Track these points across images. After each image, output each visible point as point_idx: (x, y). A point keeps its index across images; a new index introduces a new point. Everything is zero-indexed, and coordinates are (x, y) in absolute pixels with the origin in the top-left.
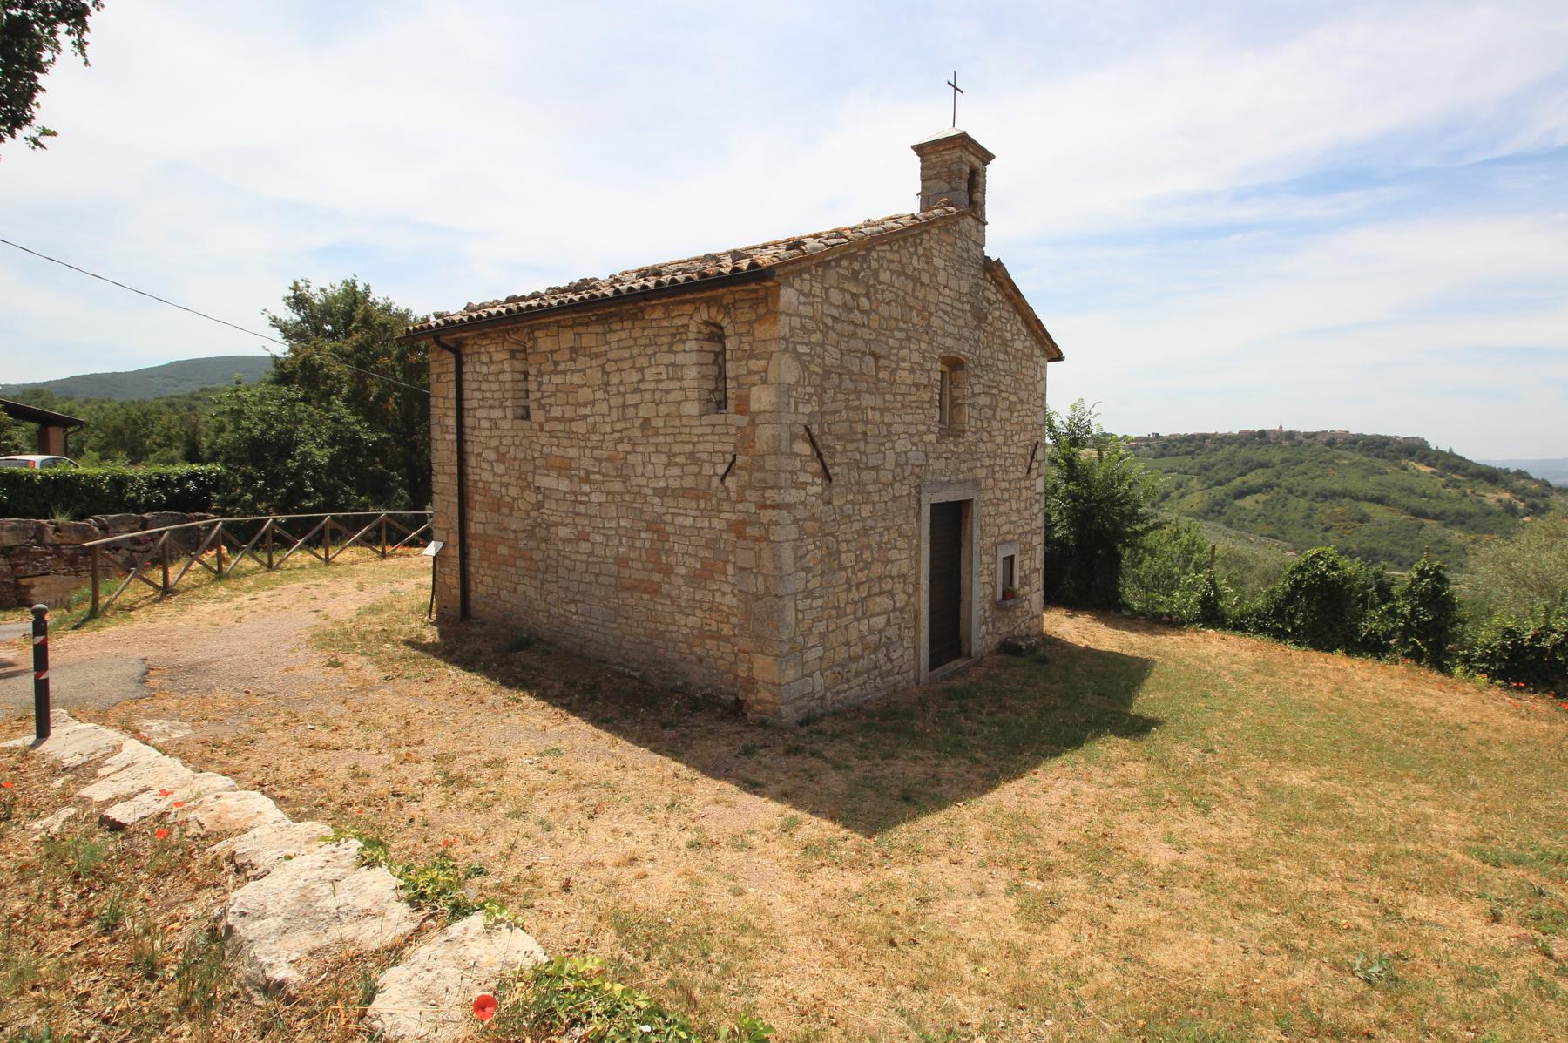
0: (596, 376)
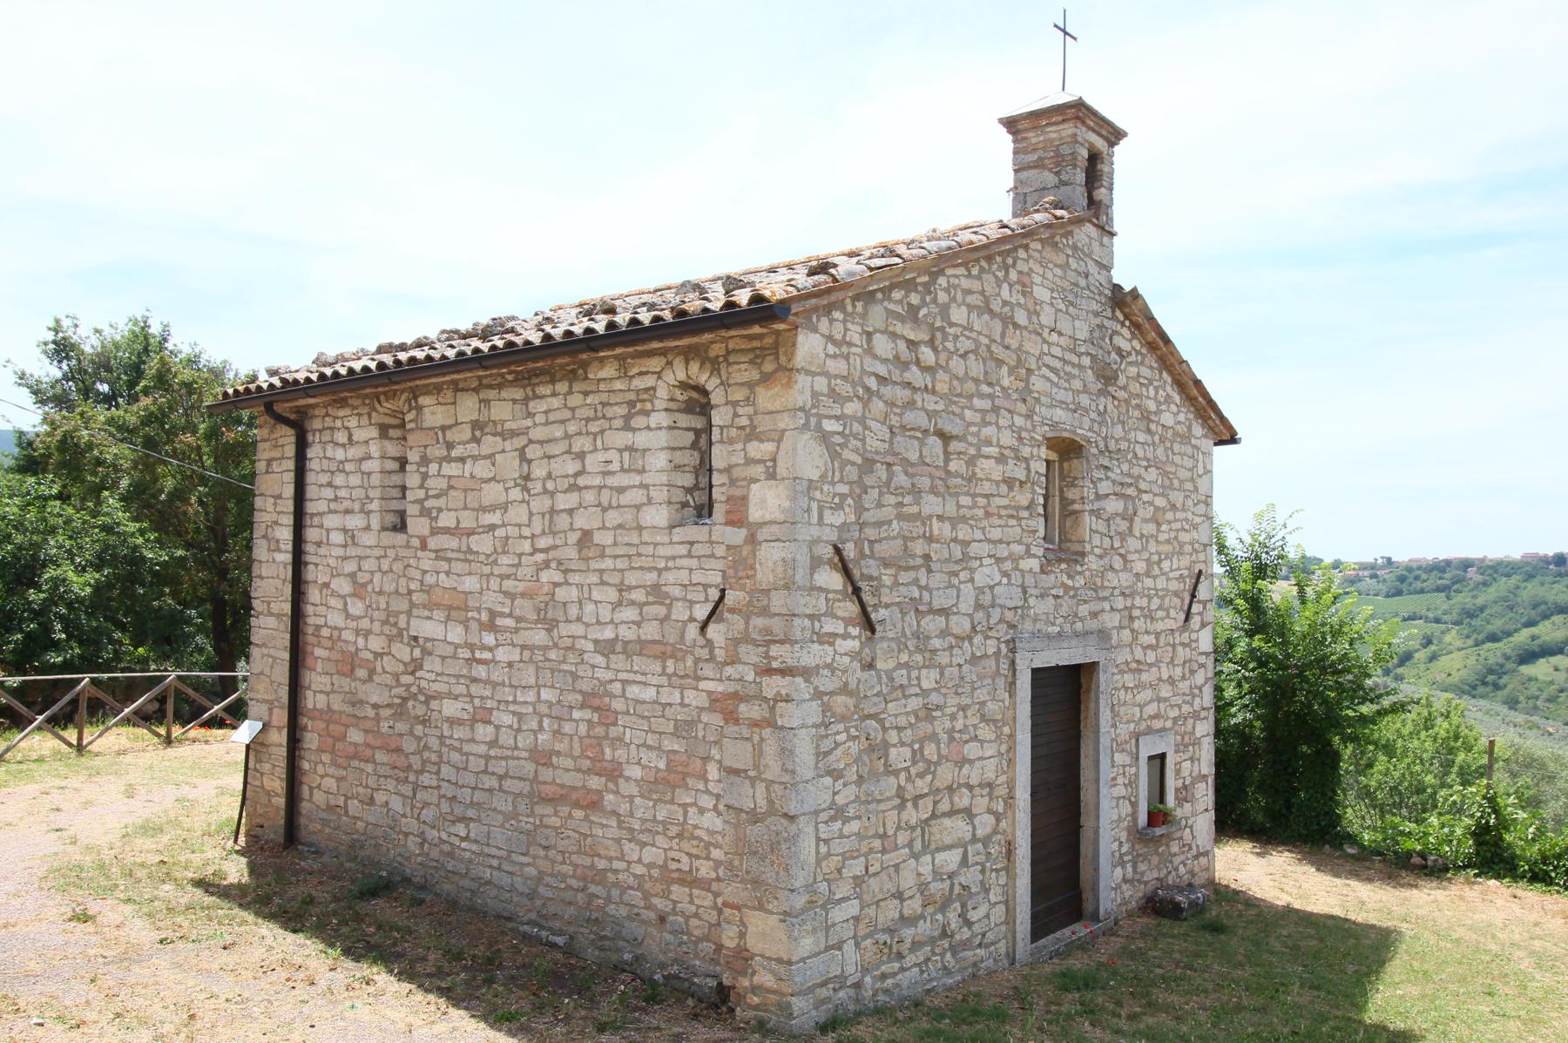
0: (510, 465)
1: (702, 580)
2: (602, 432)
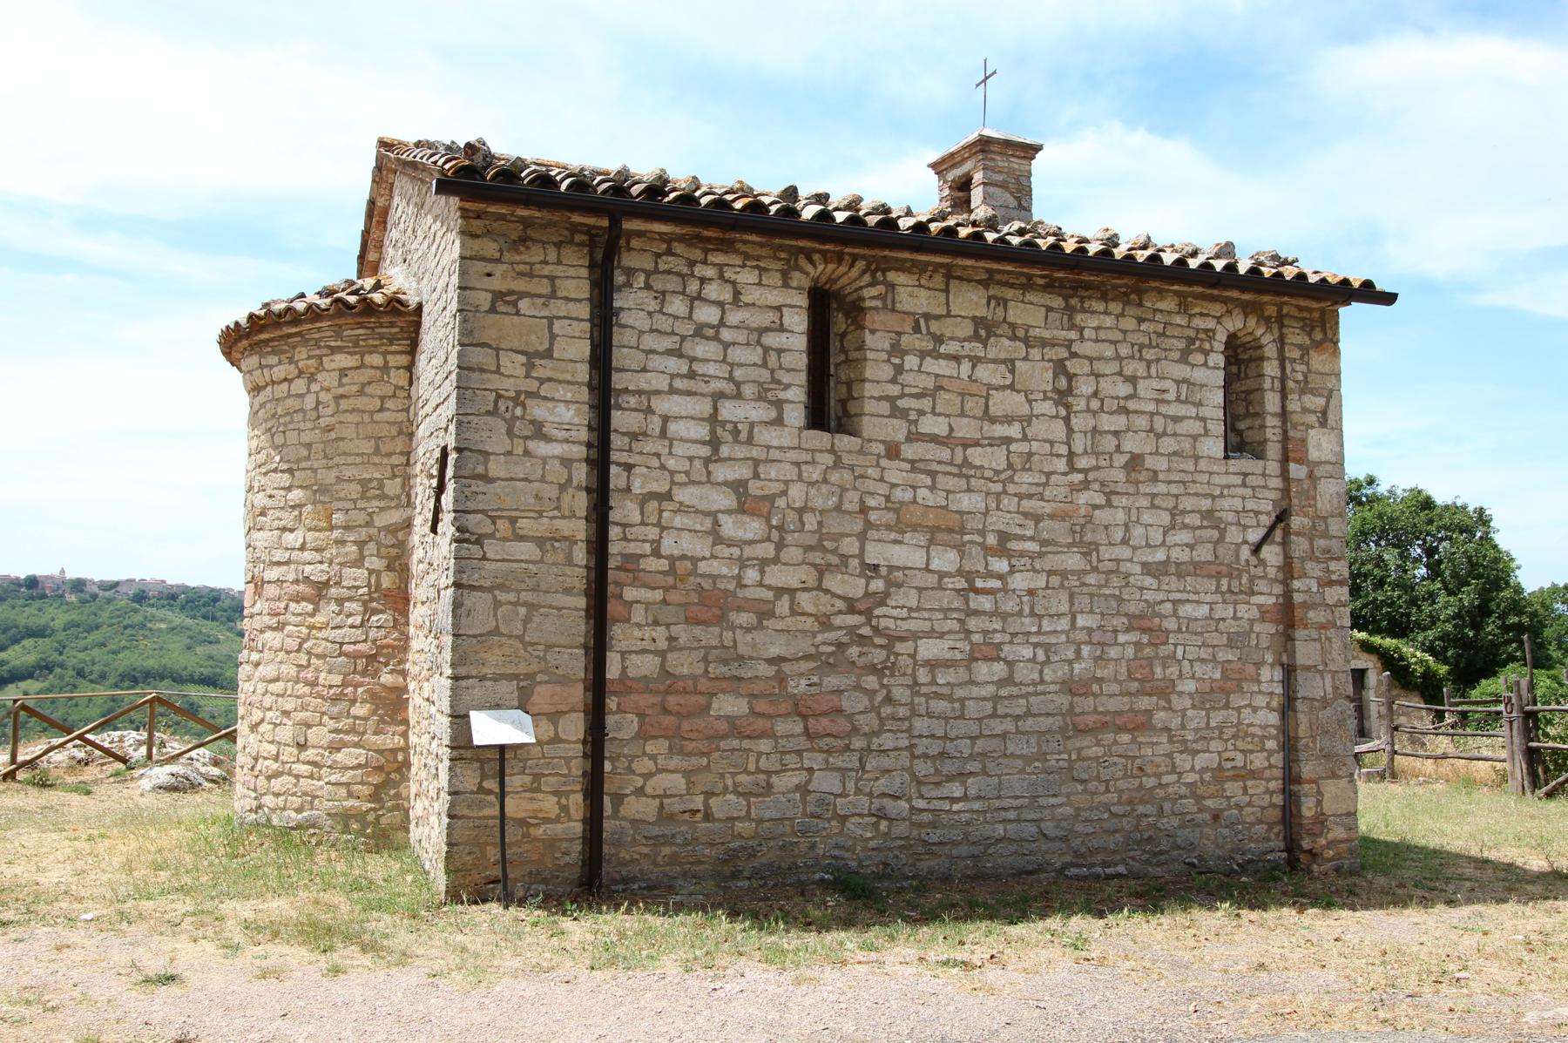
0: (1036, 372)
1: (1255, 508)
2: (1158, 360)
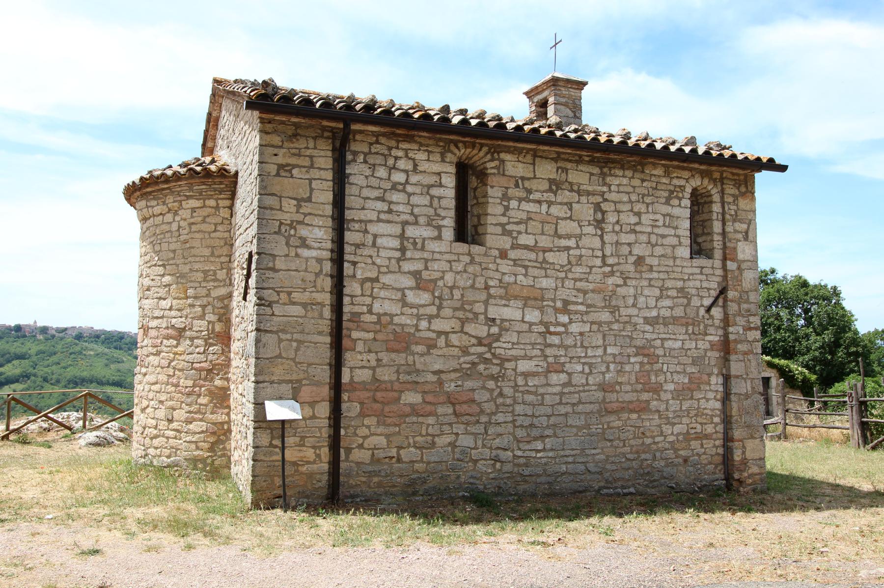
0: (584, 210)
1: (708, 286)
2: (653, 203)
